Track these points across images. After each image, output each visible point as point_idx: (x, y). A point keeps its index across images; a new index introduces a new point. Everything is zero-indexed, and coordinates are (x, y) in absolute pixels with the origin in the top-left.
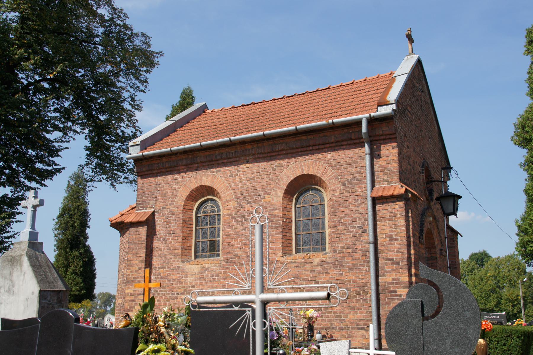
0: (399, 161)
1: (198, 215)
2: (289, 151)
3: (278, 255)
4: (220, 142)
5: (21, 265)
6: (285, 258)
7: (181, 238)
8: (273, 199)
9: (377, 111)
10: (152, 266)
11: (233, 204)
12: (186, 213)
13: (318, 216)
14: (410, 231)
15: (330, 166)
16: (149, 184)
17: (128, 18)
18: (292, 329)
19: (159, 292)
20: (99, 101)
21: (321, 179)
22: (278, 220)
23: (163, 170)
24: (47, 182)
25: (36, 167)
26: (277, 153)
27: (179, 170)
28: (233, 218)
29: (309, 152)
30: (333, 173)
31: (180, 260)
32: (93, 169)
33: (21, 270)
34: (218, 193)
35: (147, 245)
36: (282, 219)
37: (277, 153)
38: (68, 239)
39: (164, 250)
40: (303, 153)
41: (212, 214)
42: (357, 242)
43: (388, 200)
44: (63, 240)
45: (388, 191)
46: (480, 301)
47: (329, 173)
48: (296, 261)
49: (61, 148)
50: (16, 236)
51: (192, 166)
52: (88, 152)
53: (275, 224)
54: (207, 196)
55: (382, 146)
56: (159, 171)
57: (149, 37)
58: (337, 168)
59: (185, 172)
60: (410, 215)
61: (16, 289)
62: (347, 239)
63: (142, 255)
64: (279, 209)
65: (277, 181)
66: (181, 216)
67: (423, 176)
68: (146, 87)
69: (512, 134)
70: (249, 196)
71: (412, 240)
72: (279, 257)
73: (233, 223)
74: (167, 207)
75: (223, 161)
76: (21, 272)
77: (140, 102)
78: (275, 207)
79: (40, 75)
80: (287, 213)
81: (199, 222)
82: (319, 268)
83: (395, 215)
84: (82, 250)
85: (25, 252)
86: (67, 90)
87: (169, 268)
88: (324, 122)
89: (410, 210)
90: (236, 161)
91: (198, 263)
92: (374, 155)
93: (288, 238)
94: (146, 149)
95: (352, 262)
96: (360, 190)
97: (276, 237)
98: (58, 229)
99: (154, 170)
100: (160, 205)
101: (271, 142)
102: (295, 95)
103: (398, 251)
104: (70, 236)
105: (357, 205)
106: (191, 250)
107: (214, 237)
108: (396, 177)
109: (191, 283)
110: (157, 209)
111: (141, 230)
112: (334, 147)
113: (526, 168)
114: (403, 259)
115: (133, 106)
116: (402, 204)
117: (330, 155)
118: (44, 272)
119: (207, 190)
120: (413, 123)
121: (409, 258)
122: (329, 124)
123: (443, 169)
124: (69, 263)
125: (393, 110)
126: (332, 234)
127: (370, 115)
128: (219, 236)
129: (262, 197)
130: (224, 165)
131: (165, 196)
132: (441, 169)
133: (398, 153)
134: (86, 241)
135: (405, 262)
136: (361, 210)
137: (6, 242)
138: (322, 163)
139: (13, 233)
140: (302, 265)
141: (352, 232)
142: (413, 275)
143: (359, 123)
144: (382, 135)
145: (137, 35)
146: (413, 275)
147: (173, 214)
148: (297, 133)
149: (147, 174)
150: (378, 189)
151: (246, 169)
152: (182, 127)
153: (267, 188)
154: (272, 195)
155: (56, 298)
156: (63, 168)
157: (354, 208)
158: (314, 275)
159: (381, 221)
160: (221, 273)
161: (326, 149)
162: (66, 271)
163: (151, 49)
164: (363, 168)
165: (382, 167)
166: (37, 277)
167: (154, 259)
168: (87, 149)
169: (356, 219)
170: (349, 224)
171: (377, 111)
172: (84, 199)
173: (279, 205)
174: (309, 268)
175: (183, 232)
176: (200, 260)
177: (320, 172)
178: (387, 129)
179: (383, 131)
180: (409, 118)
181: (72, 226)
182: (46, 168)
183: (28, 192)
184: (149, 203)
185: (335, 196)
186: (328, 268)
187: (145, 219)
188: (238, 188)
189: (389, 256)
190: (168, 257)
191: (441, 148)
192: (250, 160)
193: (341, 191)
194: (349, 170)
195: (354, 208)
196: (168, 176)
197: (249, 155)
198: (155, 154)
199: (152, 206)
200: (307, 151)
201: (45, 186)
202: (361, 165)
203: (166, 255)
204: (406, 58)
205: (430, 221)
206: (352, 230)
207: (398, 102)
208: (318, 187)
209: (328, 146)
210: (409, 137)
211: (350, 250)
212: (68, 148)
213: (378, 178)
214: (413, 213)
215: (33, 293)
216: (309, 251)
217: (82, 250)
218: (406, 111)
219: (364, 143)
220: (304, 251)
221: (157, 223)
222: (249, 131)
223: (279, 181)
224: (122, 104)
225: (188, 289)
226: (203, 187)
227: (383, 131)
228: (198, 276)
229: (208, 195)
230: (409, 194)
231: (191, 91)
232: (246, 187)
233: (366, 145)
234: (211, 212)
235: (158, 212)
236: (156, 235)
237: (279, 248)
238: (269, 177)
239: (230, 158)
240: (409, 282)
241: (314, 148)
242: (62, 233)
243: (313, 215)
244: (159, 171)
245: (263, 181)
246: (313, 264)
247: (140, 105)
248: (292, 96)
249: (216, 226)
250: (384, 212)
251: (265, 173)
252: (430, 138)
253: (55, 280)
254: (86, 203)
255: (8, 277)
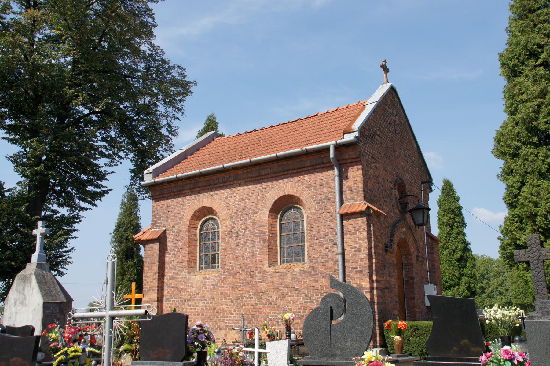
0: (364, 181)
1: (202, 232)
2: (273, 175)
3: (265, 266)
4: (215, 169)
5: (30, 282)
6: (271, 268)
7: (187, 252)
8: (260, 217)
9: (343, 138)
10: (164, 277)
11: (228, 222)
12: (191, 230)
13: (299, 230)
14: (372, 243)
15: (307, 187)
16: (161, 206)
17: (165, 53)
18: (244, 331)
19: (170, 300)
20: (140, 129)
21: (300, 199)
22: (265, 235)
23: (172, 194)
24: (97, 202)
25: (88, 189)
26: (264, 177)
27: (185, 193)
28: (229, 234)
29: (289, 175)
30: (309, 194)
31: (186, 271)
32: (137, 189)
33: (31, 286)
34: (216, 213)
35: (159, 259)
36: (268, 234)
37: (264, 177)
38: (123, 250)
39: (174, 263)
40: (285, 176)
41: (213, 231)
42: (329, 253)
43: (353, 216)
44: (119, 251)
45: (353, 208)
46: (518, 297)
47: (306, 193)
48: (280, 270)
49: (106, 172)
50: (72, 251)
51: (195, 190)
52: (133, 174)
53: (263, 239)
54: (208, 215)
55: (350, 168)
56: (169, 195)
57: (184, 69)
58: (312, 188)
59: (190, 195)
60: (372, 228)
61: (27, 302)
62: (321, 250)
63: (155, 268)
64: (265, 226)
65: (264, 201)
66: (187, 234)
67: (396, 193)
68: (183, 114)
69: (493, 148)
70: (242, 215)
71: (373, 250)
72: (266, 268)
73: (229, 239)
74: (176, 226)
75: (220, 185)
76: (31, 288)
77: (176, 128)
78: (263, 224)
79: (90, 109)
80: (273, 229)
81: (203, 238)
82: (299, 276)
83: (359, 229)
84: (135, 260)
85: (33, 272)
86: (111, 121)
87: (178, 278)
88: (299, 150)
89: (372, 225)
90: (231, 185)
91: (201, 274)
92: (343, 177)
93: (274, 251)
94: (158, 176)
95: (325, 271)
96: (331, 208)
97: (263, 251)
98: (114, 241)
99: (165, 194)
100: (170, 224)
101: (258, 167)
102: (289, 122)
103: (361, 261)
104: (125, 248)
105: (329, 221)
106: (196, 262)
107: (215, 251)
108: (361, 196)
109: (195, 291)
110: (168, 228)
111: (155, 246)
112: (310, 170)
113: (503, 178)
114: (365, 267)
115: (170, 132)
116: (364, 219)
117: (307, 178)
118: (48, 287)
119: (207, 210)
120: (384, 146)
121: (371, 266)
122: (303, 151)
123: (422, 183)
124: (125, 272)
125: (356, 137)
126: (310, 246)
127: (336, 142)
128: (218, 250)
129: (252, 215)
130: (221, 188)
131: (174, 216)
132: (420, 183)
133: (363, 174)
134: (140, 252)
135: (367, 270)
136: (332, 225)
137: (65, 256)
138: (300, 184)
139: (70, 248)
140: (285, 274)
141: (325, 244)
142: (375, 281)
143: (327, 149)
144: (349, 159)
145: (174, 67)
146: (375, 281)
147: (181, 232)
148: (278, 159)
149: (160, 198)
150: (346, 206)
151: (239, 192)
152: (192, 154)
153: (256, 207)
154: (260, 214)
155: (58, 308)
156: (110, 190)
157: (327, 224)
158: (294, 283)
159: (347, 234)
160: (219, 282)
161: (304, 173)
162: (123, 279)
163: (186, 79)
164: (333, 188)
165: (349, 187)
166: (41, 292)
167: (166, 271)
168: (132, 171)
169: (328, 233)
170: (323, 238)
171: (343, 138)
172: (136, 214)
173: (266, 222)
174: (290, 276)
175: (189, 247)
176: (203, 271)
177: (299, 193)
178: (352, 153)
179: (349, 155)
180: (379, 141)
181: (127, 238)
182: (96, 190)
183: (81, 212)
184: (161, 223)
185: (311, 214)
186: (306, 277)
187: (157, 237)
188: (233, 208)
189: (353, 265)
190: (177, 269)
191: (422, 164)
192: (242, 184)
193: (316, 209)
194: (322, 190)
195: (327, 224)
196: (176, 199)
197: (241, 179)
198: (164, 180)
199: (164, 225)
200: (288, 174)
201: (96, 205)
202: (332, 185)
203: (175, 267)
204: (381, 86)
205: (404, 231)
206: (324, 243)
207: (362, 130)
208: (298, 206)
209: (305, 169)
210: (378, 158)
211: (323, 261)
212: (114, 172)
213: (346, 197)
214: (376, 226)
215: (39, 305)
216: (291, 261)
217: (135, 260)
218: (374, 135)
219: (333, 166)
220: (287, 262)
221: (168, 240)
222: (240, 158)
223: (265, 201)
224: (160, 131)
225: (193, 296)
226: (204, 207)
227: (349, 155)
228: (201, 285)
229: (210, 214)
230: (371, 211)
231: (214, 118)
232: (239, 207)
233: (336, 169)
234: (212, 230)
235: (168, 230)
236: (167, 250)
237: (266, 260)
238: (257, 198)
239: (226, 182)
240: (370, 287)
241: (293, 171)
242: (118, 245)
243: (295, 230)
244: (169, 195)
245: (253, 201)
246: (294, 273)
247: (176, 131)
248: (286, 123)
249: (216, 241)
250: (350, 226)
251: (254, 195)
252: (406, 156)
253: (57, 294)
254: (139, 218)
255: (22, 292)
